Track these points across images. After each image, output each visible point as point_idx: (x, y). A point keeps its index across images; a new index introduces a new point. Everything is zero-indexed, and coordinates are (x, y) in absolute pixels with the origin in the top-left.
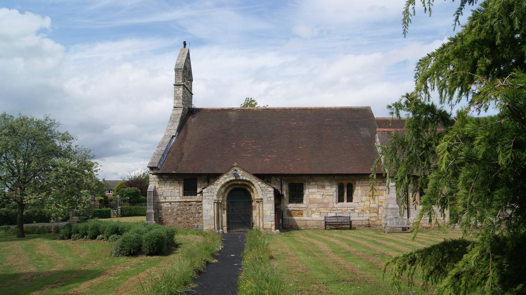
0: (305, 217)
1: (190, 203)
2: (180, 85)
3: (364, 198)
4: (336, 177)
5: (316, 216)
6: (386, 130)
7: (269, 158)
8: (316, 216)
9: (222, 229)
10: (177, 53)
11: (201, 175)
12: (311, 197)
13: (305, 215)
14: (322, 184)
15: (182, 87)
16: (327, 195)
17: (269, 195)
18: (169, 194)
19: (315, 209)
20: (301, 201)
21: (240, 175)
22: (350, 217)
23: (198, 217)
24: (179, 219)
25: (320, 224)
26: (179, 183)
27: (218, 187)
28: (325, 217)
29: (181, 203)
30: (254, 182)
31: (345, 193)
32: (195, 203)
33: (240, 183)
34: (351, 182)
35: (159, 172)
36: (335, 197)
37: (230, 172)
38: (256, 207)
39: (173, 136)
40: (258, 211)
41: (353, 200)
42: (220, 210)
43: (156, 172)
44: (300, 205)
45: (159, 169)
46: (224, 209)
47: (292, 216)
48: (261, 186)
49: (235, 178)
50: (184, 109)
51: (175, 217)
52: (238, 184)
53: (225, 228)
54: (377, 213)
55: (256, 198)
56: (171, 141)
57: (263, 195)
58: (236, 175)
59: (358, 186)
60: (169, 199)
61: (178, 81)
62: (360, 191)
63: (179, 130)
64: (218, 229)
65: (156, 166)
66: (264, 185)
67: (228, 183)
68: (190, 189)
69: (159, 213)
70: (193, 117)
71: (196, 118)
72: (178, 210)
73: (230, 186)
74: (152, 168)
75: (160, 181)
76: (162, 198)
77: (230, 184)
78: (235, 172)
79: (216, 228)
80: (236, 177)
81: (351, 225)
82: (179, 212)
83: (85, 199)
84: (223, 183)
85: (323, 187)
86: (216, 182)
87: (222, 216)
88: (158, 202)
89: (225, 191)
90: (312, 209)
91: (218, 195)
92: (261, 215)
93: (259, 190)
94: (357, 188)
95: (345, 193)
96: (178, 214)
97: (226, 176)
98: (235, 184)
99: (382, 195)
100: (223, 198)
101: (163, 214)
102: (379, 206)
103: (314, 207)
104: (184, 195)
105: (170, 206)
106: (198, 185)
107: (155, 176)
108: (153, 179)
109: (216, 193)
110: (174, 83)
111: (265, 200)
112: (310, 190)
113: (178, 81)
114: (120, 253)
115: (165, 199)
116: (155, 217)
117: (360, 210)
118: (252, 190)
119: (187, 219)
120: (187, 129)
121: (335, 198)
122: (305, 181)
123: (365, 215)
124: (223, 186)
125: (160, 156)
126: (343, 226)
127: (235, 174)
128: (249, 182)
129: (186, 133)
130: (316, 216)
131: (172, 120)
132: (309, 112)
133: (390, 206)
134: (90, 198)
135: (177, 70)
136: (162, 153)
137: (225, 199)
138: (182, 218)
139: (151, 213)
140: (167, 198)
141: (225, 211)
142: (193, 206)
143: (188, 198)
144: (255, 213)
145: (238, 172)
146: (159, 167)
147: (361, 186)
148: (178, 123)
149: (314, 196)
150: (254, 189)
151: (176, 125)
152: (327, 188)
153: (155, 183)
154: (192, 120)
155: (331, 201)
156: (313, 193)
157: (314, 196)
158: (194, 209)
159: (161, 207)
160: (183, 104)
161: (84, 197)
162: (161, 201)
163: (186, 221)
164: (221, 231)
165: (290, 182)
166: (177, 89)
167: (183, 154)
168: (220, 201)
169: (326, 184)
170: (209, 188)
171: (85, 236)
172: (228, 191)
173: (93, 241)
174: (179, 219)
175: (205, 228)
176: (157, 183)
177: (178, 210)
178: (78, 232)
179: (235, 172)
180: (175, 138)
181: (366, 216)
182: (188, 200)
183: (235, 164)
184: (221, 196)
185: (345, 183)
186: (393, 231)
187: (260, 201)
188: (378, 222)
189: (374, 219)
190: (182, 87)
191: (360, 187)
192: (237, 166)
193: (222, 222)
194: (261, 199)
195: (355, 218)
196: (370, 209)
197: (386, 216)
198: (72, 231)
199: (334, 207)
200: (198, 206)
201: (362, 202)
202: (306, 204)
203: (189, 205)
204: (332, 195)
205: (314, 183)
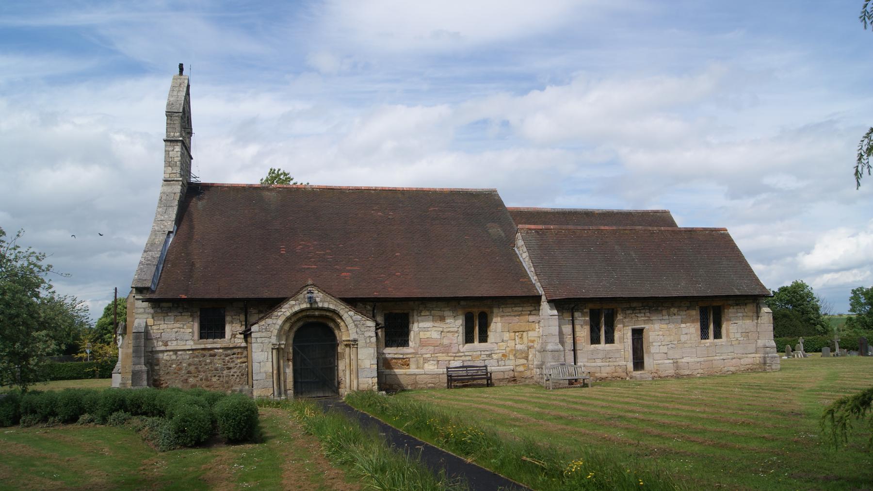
0: (413, 370)
1: (212, 352)
2: (177, 141)
3: (506, 336)
4: (462, 303)
5: (430, 367)
6: (533, 227)
7: (349, 271)
8: (432, 367)
9: (286, 394)
10: (166, 84)
11: (232, 301)
12: (422, 335)
13: (413, 366)
14: (440, 313)
15: (180, 144)
16: (448, 332)
17: (367, 334)
18: (173, 336)
19: (429, 355)
20: (405, 343)
21: (318, 300)
22: (486, 366)
23: (228, 376)
24: (192, 380)
25: (437, 380)
26: (191, 316)
27: (280, 322)
28: (448, 368)
29: (196, 353)
30: (342, 312)
31: (477, 327)
32: (221, 351)
33: (317, 313)
34: (486, 310)
35: (154, 296)
36: (461, 334)
37: (301, 296)
38: (343, 354)
39: (170, 232)
40: (348, 361)
41: (489, 340)
42: (282, 362)
43: (148, 296)
44: (405, 350)
45: (153, 292)
46: (288, 360)
47: (392, 368)
48: (354, 318)
49: (309, 306)
50: (183, 185)
51: (185, 377)
52: (314, 316)
53: (291, 392)
54: (526, 358)
55: (344, 338)
56: (166, 242)
57: (358, 332)
58: (311, 300)
59: (497, 316)
60: (173, 345)
61: (172, 134)
62: (499, 325)
63: (179, 220)
64: (280, 394)
65: (148, 284)
66: (359, 317)
67: (296, 313)
68: (212, 327)
69: (153, 370)
70: (200, 199)
71: (204, 201)
72: (189, 365)
73: (299, 320)
74: (139, 290)
75: (155, 312)
76: (161, 343)
77: (300, 315)
78: (309, 295)
79: (276, 393)
80: (311, 304)
81: (490, 379)
82: (192, 368)
83: (44, 349)
84: (288, 314)
85: (442, 319)
86: (276, 313)
87: (285, 373)
88: (152, 352)
89: (291, 328)
90: (425, 356)
91: (279, 336)
92: (354, 367)
93: (351, 326)
94: (494, 320)
95: (477, 327)
96: (189, 372)
97: (293, 302)
98: (308, 316)
99: (534, 330)
100: (286, 340)
101: (162, 373)
102: (529, 348)
103: (427, 352)
104: (201, 337)
105: (174, 357)
106: (228, 318)
107: (146, 304)
108: (142, 310)
109: (275, 332)
110: (165, 138)
111: (361, 343)
112: (422, 325)
113: (172, 134)
114: (176, 444)
115: (166, 345)
116: (148, 380)
117: (500, 355)
118: (338, 326)
119: (207, 380)
120: (191, 221)
121: (461, 338)
122: (413, 310)
123: (507, 362)
124: (288, 319)
125: (154, 269)
126: (475, 382)
127: (310, 298)
128: (334, 311)
129: (191, 227)
130: (432, 367)
131: (163, 203)
132: (400, 196)
133: (550, 347)
134: (53, 346)
135: (170, 114)
136: (156, 262)
137: (291, 341)
138: (198, 379)
139: (141, 371)
140: (169, 343)
141: (291, 363)
142: (217, 357)
143: (209, 343)
144: (342, 365)
145: (314, 295)
146: (153, 287)
147: (502, 316)
148: (176, 208)
149: (428, 334)
150: (342, 324)
151: (173, 213)
152: (448, 321)
153: (146, 316)
154: (198, 205)
155: (455, 341)
156: (426, 330)
157: (428, 334)
158: (221, 362)
159: (158, 360)
160: (181, 176)
161: (41, 345)
162: (158, 349)
163: (205, 383)
164: (283, 397)
165: (387, 312)
166: (171, 149)
167: (193, 264)
168: (283, 346)
169: (447, 313)
170: (263, 323)
171: (51, 419)
172: (295, 329)
173: (70, 426)
174: (192, 380)
175: (256, 393)
176: (150, 316)
177: (189, 365)
178: (34, 412)
179: (309, 295)
180: (172, 236)
181: (510, 365)
182: (209, 346)
183: (310, 282)
184: (284, 338)
185: (476, 311)
186: (557, 387)
187: (353, 344)
188: (528, 374)
189: (521, 369)
190: (180, 144)
191: (499, 319)
192: (314, 285)
193: (285, 382)
194: (355, 340)
195: (493, 367)
196: (516, 353)
197: (543, 363)
198: (21, 410)
199: (459, 351)
200: (227, 355)
201: (503, 341)
202: (414, 348)
203: (211, 355)
204: (457, 332)
205: (428, 313)
